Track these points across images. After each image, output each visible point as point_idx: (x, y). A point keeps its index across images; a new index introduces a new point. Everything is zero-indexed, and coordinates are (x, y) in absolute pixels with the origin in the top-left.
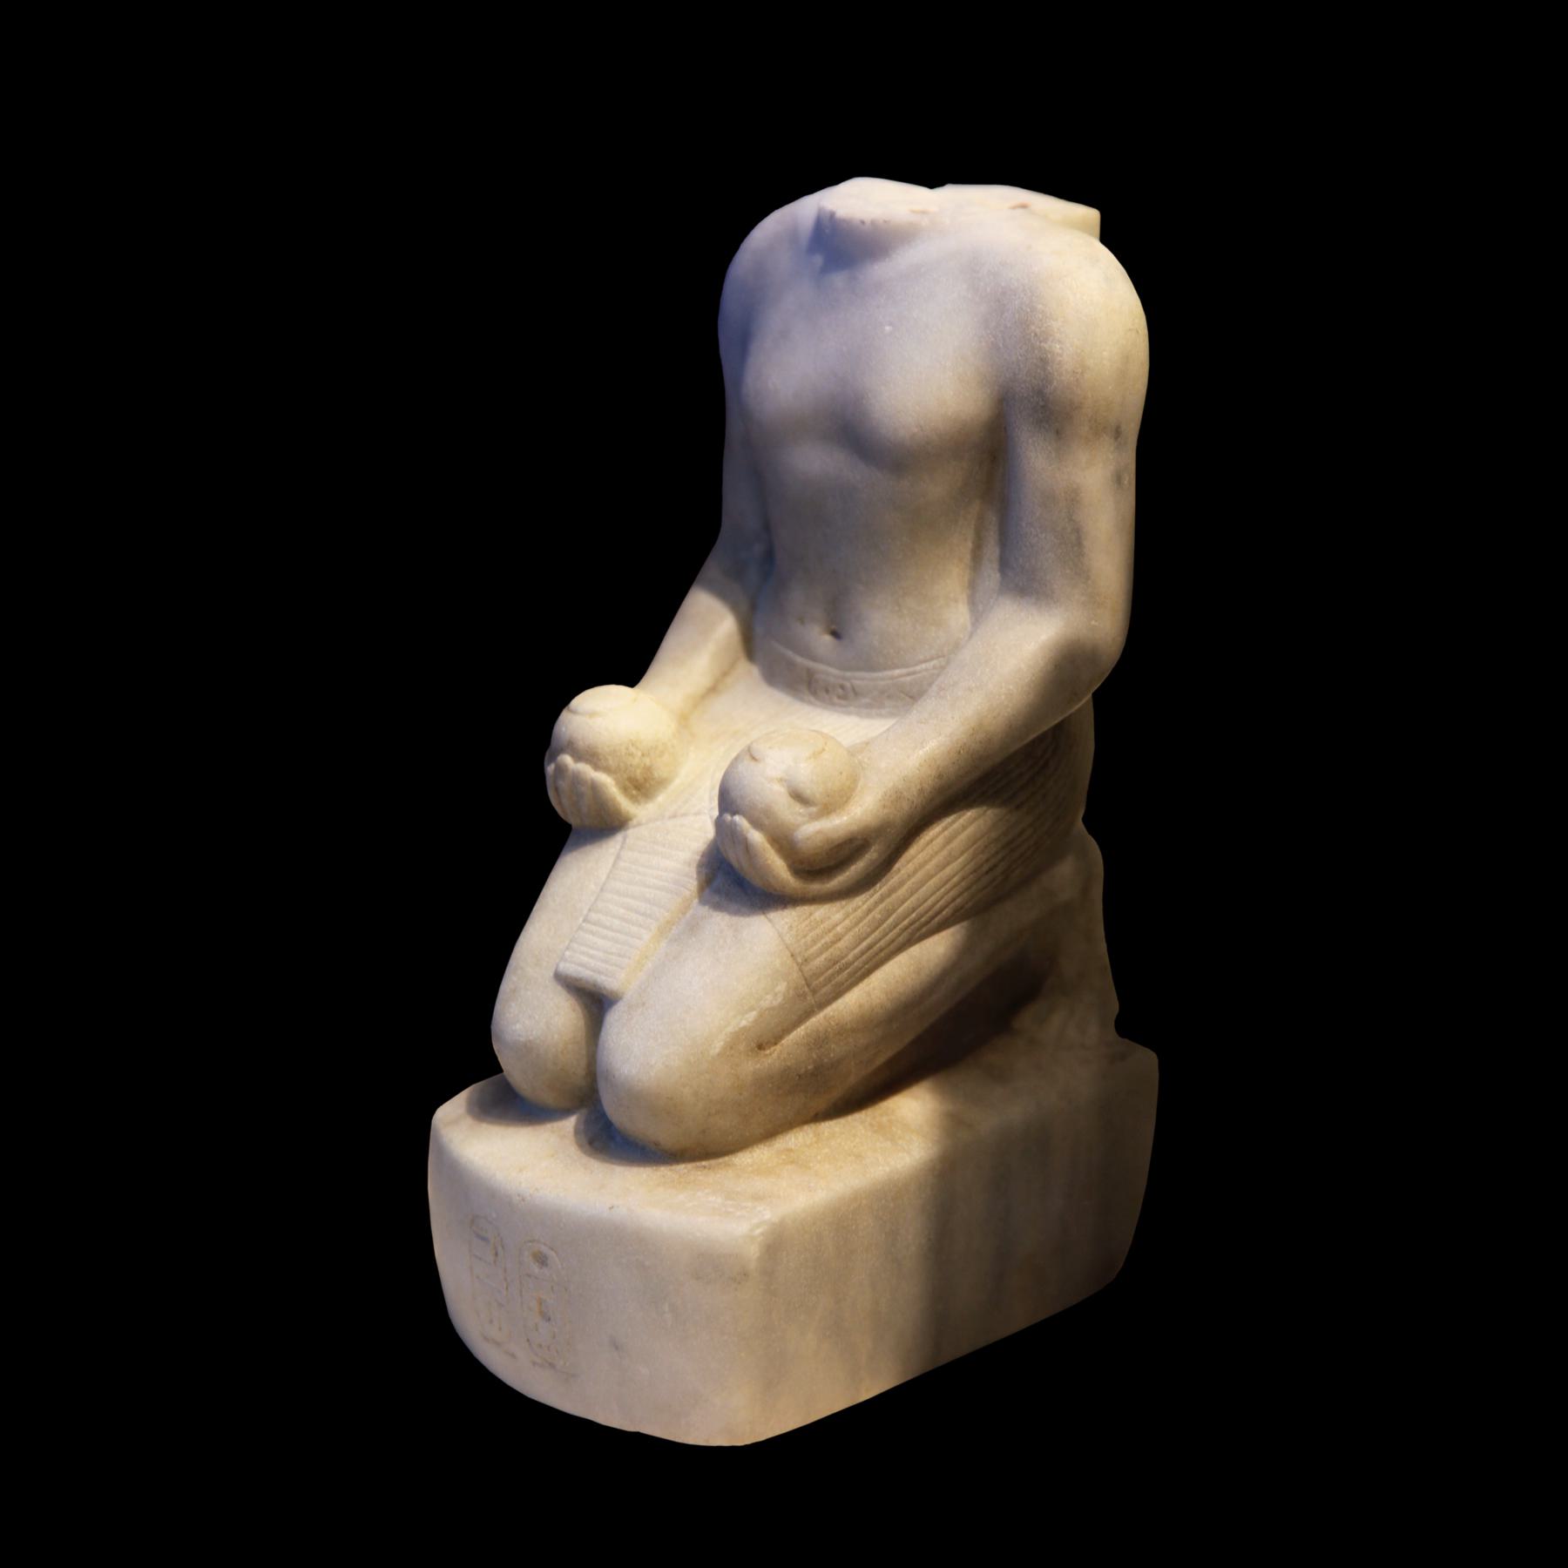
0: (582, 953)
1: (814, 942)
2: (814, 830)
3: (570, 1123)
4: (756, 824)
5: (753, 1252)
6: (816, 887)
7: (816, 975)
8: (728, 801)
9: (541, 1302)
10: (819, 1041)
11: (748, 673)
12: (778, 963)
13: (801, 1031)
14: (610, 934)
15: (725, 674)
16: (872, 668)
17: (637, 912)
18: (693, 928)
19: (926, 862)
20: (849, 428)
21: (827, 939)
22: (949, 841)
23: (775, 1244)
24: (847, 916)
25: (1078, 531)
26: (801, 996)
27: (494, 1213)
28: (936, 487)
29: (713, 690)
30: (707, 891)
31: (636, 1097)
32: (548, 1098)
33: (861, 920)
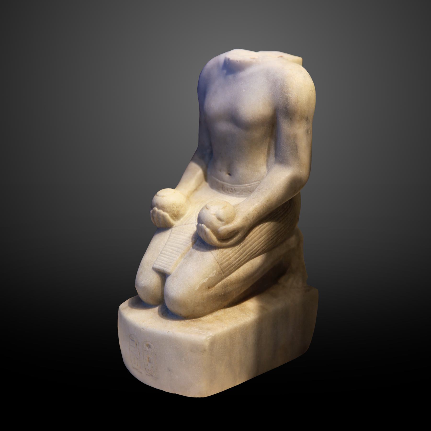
0: (160, 262)
1: (224, 259)
2: (224, 228)
3: (157, 309)
4: (208, 227)
5: (207, 344)
6: (224, 244)
7: (224, 268)
8: (200, 220)
9: (149, 358)
10: (225, 286)
11: (206, 185)
12: (214, 265)
13: (220, 283)
14: (168, 257)
15: (199, 185)
16: (240, 184)
17: (175, 251)
18: (191, 255)
19: (254, 237)
20: (233, 118)
21: (227, 258)
22: (261, 231)
23: (213, 342)
24: (233, 252)
25: (296, 146)
26: (220, 274)
27: (136, 334)
28: (257, 134)
29: (196, 190)
30: (194, 245)
31: (175, 302)
32: (151, 302)
33: (237, 253)
